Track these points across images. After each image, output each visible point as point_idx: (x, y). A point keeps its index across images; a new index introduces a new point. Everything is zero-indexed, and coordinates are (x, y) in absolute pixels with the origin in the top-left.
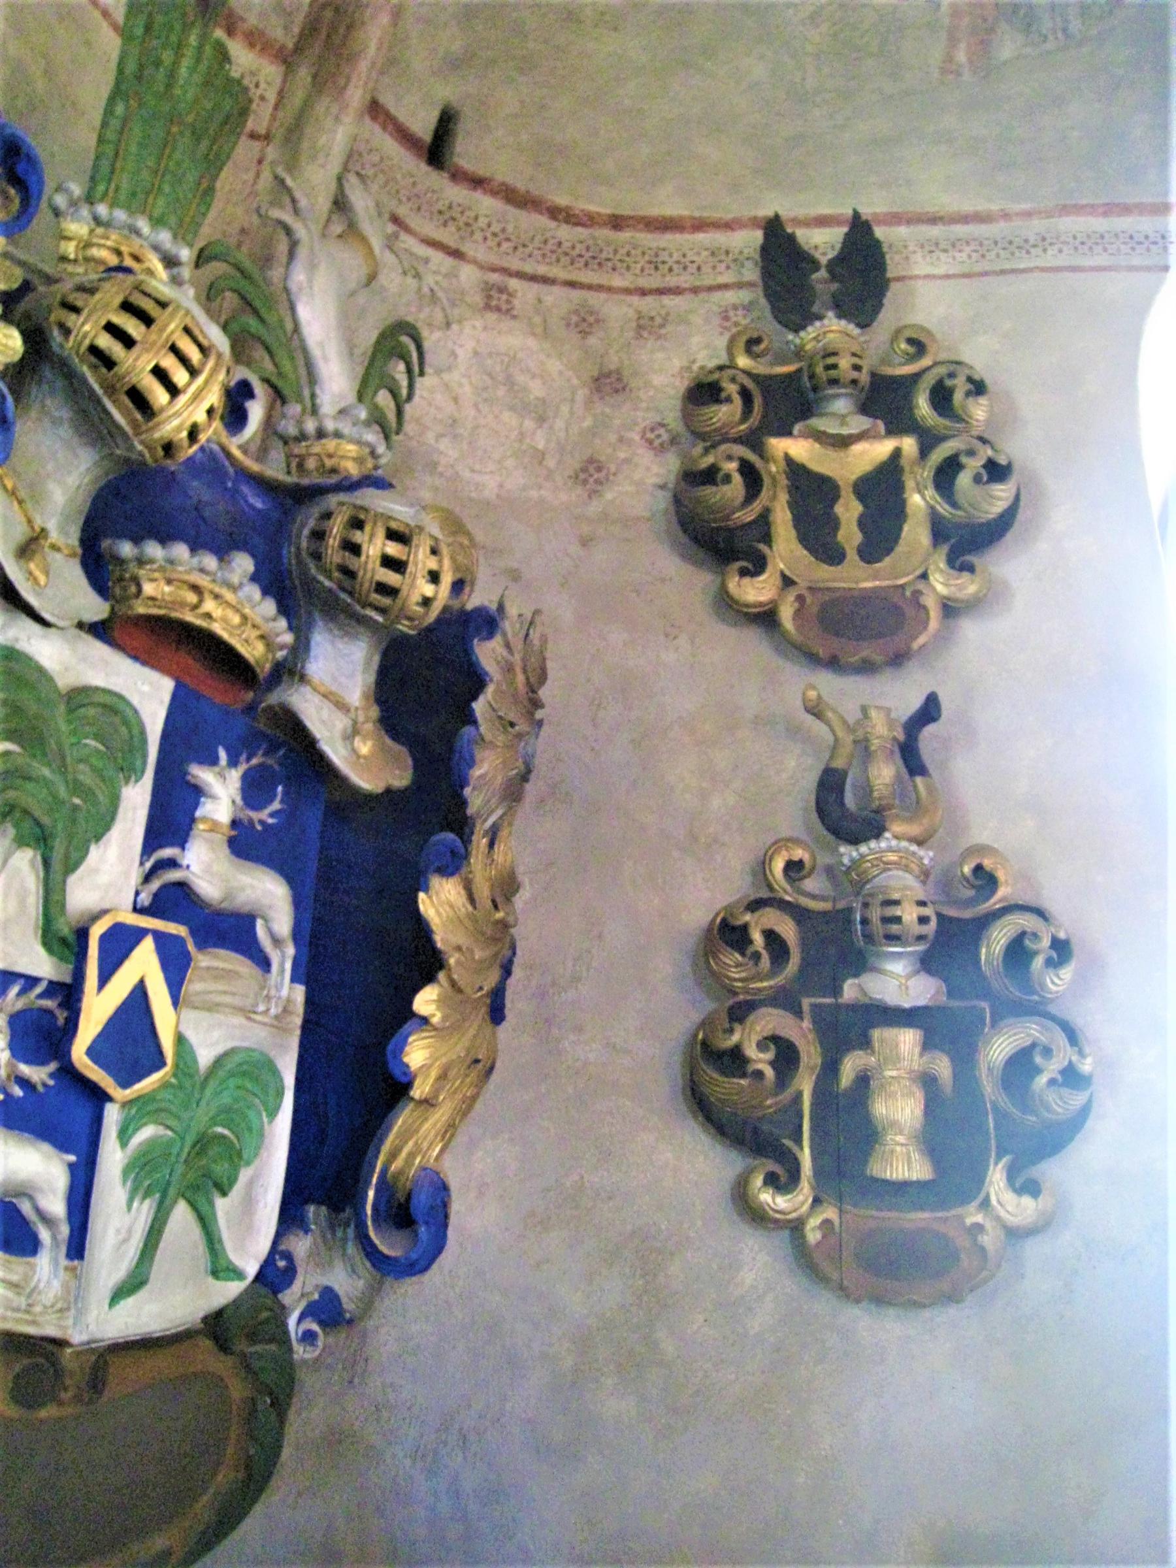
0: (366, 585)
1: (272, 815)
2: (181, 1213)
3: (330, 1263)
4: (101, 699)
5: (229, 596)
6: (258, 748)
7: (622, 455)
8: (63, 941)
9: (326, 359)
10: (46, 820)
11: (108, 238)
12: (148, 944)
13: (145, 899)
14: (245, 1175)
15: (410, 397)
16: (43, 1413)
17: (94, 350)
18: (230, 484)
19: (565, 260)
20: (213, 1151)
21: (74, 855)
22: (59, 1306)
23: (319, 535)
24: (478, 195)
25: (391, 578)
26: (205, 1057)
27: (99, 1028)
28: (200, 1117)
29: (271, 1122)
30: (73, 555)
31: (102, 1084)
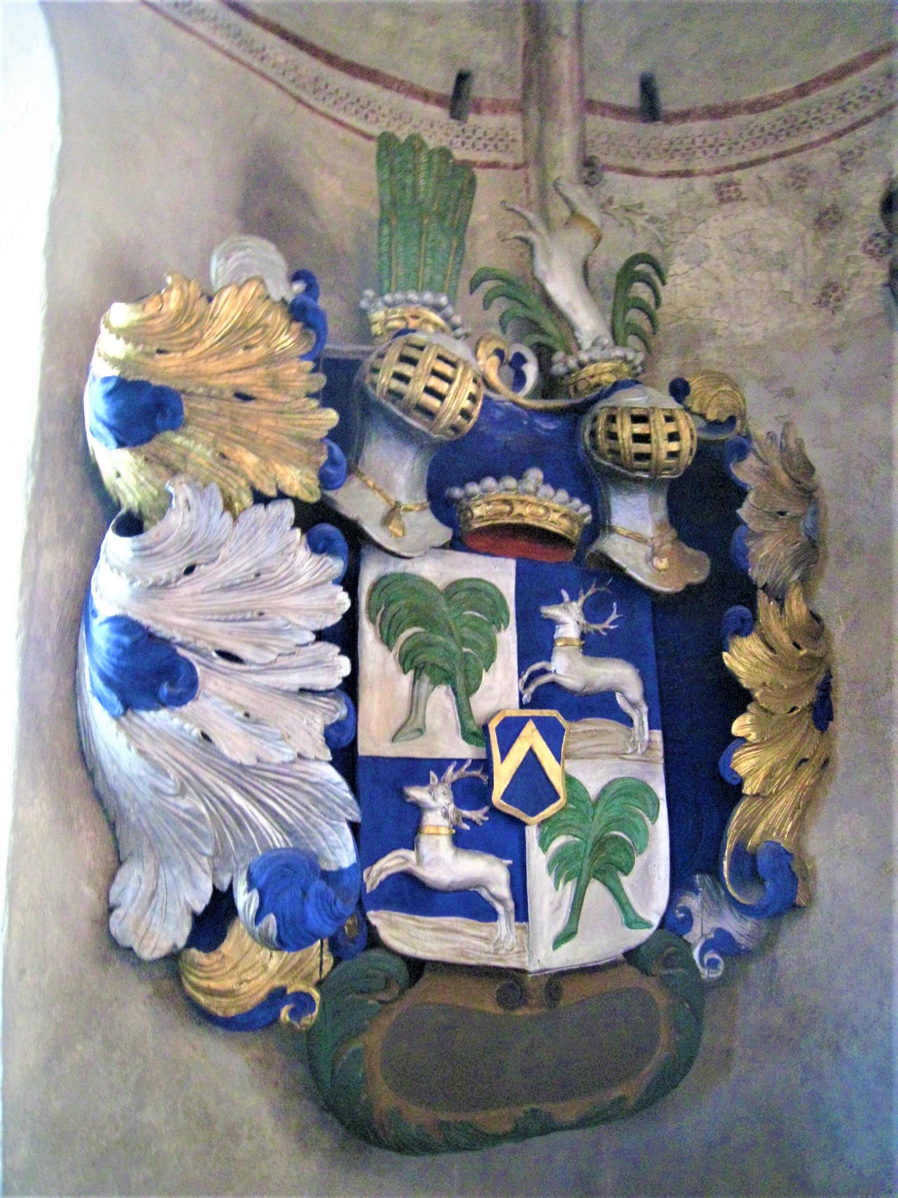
0: (628, 458)
1: (612, 623)
2: (595, 889)
3: (720, 912)
4: (467, 585)
5: (531, 499)
6: (591, 583)
7: (851, 271)
8: (475, 734)
9: (575, 312)
10: (447, 666)
11: (395, 313)
12: (530, 726)
13: (527, 698)
14: (639, 861)
15: (658, 304)
16: (519, 1013)
17: (390, 392)
18: (525, 423)
19: (771, 139)
20: (610, 847)
21: (473, 683)
22: (516, 949)
23: (593, 434)
24: (689, 124)
25: (644, 448)
26: (593, 789)
27: (508, 782)
28: (595, 828)
29: (653, 823)
30: (423, 508)
31: (517, 816)
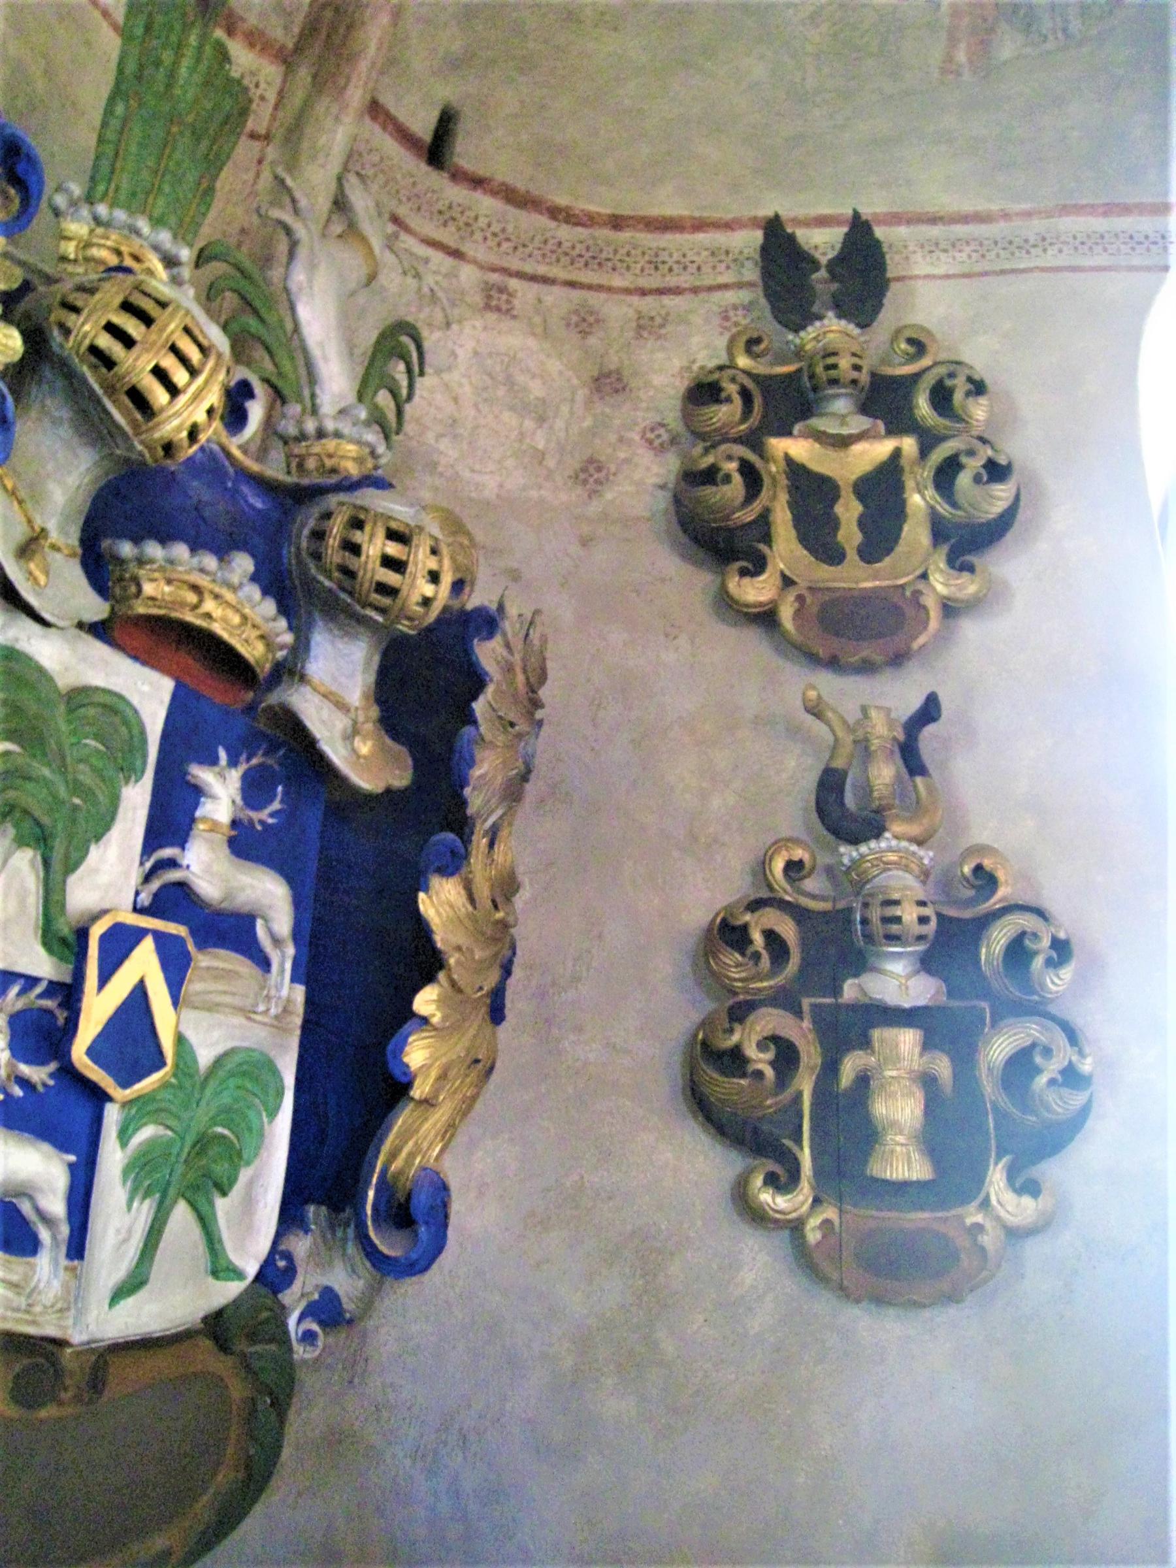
0: (366, 585)
1: (272, 815)
2: (181, 1213)
3: (330, 1263)
4: (101, 699)
5: (229, 596)
6: (258, 748)
7: (622, 455)
8: (63, 941)
9: (326, 359)
10: (46, 820)
11: (108, 238)
12: (148, 944)
13: (145, 899)
14: (245, 1175)
15: (410, 397)
16: (43, 1413)
17: (94, 350)
18: (230, 484)
19: (565, 260)
20: (213, 1151)
21: (74, 855)
22: (59, 1306)
23: (319, 535)
24: (478, 195)
25: (391, 578)
26: (205, 1057)
27: (99, 1028)
28: (200, 1117)
29: (271, 1122)
30: (73, 555)
31: (102, 1084)
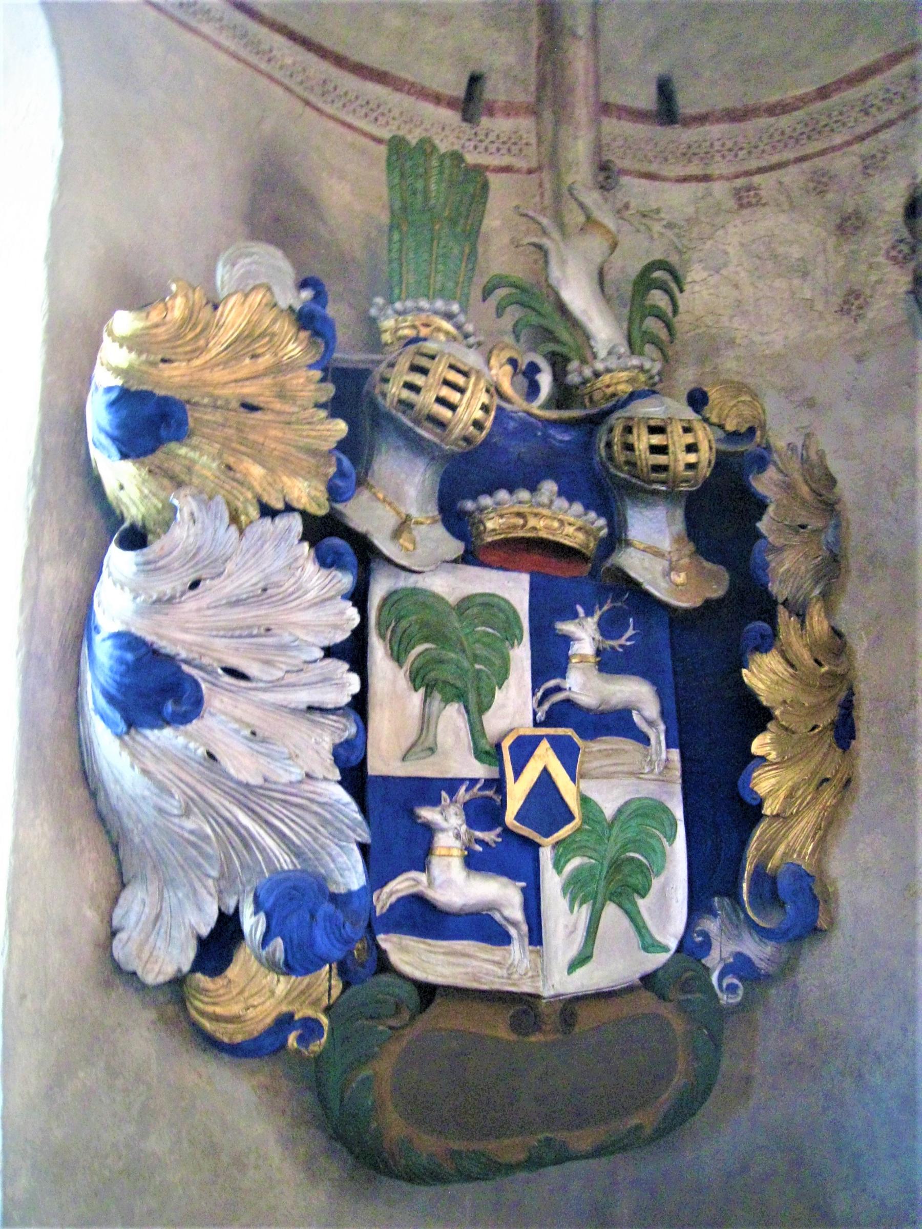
0: (645, 470)
1: (629, 639)
2: (611, 912)
3: (739, 936)
4: (479, 600)
5: (545, 512)
6: (607, 598)
7: (873, 278)
8: (487, 753)
9: (590, 320)
10: (459, 684)
11: (406, 321)
12: (545, 745)
13: (541, 716)
14: (656, 883)
15: (675, 312)
16: (533, 1039)
17: (401, 402)
18: (539, 434)
19: (791, 143)
20: (626, 869)
21: (486, 700)
22: (530, 974)
23: (609, 445)
24: (707, 127)
25: (661, 459)
26: (609, 809)
27: (521, 802)
28: (611, 850)
29: (671, 845)
30: (434, 522)
31: (531, 837)
